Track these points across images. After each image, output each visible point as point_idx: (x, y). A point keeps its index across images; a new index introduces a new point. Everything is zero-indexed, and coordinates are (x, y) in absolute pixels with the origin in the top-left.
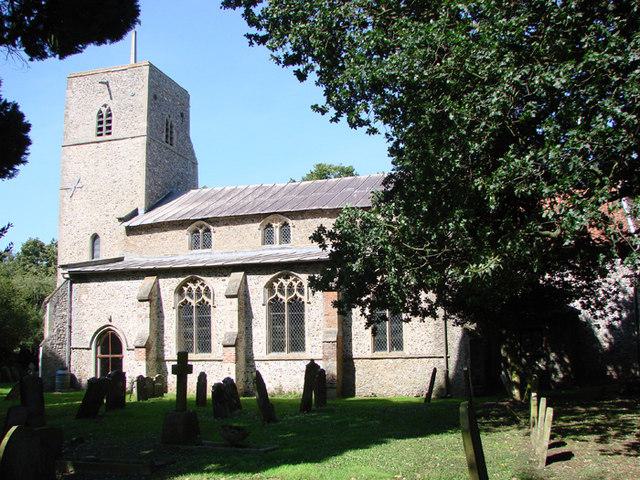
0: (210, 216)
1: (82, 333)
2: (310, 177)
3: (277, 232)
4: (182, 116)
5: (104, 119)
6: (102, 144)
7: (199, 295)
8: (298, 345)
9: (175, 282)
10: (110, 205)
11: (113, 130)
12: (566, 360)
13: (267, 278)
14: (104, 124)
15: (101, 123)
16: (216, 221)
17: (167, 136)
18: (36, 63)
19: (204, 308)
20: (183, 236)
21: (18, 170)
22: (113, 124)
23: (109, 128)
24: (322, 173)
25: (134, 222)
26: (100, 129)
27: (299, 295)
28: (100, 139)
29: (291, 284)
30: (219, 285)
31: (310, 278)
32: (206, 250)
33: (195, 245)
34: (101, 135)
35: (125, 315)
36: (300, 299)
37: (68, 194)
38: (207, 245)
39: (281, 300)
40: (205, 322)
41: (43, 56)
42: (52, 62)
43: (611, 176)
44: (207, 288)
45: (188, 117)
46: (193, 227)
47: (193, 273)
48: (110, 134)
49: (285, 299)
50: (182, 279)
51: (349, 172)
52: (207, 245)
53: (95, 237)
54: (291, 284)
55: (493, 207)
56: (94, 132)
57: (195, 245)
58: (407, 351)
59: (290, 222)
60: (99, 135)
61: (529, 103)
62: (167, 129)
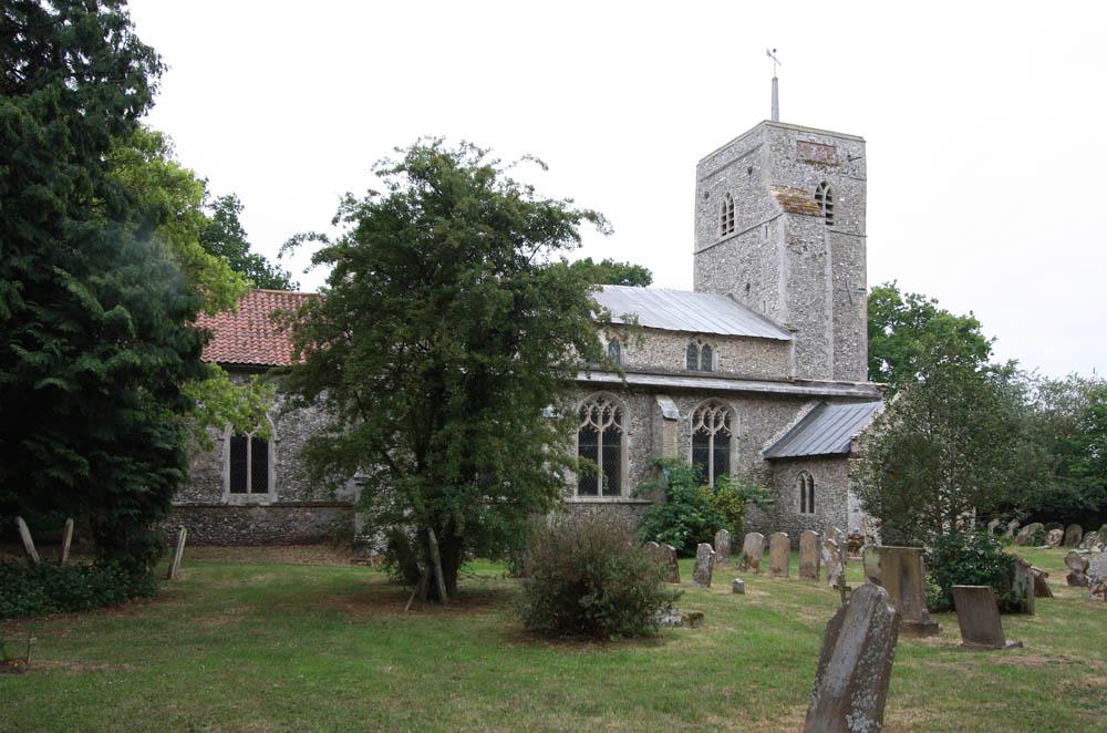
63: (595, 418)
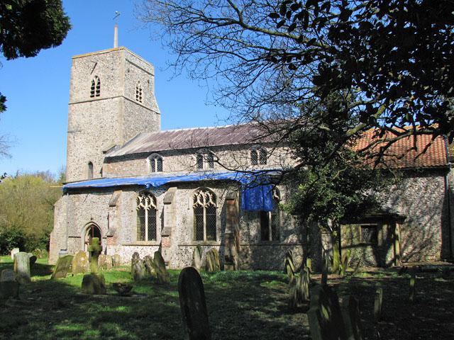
0: (161, 150)
5: (96, 89)
6: (93, 102)
10: (100, 143)
11: (101, 93)
12: (390, 33)
14: (96, 90)
15: (93, 88)
16: (166, 153)
18: (11, 61)
20: (192, 159)
22: (101, 89)
23: (98, 92)
25: (113, 154)
26: (93, 93)
28: (92, 99)
31: (325, 206)
37: (72, 136)
41: (16, 56)
42: (21, 61)
43: (367, 193)
46: (150, 156)
53: (91, 164)
55: (310, 150)
59: (164, 158)
60: (91, 97)
61: (389, 21)
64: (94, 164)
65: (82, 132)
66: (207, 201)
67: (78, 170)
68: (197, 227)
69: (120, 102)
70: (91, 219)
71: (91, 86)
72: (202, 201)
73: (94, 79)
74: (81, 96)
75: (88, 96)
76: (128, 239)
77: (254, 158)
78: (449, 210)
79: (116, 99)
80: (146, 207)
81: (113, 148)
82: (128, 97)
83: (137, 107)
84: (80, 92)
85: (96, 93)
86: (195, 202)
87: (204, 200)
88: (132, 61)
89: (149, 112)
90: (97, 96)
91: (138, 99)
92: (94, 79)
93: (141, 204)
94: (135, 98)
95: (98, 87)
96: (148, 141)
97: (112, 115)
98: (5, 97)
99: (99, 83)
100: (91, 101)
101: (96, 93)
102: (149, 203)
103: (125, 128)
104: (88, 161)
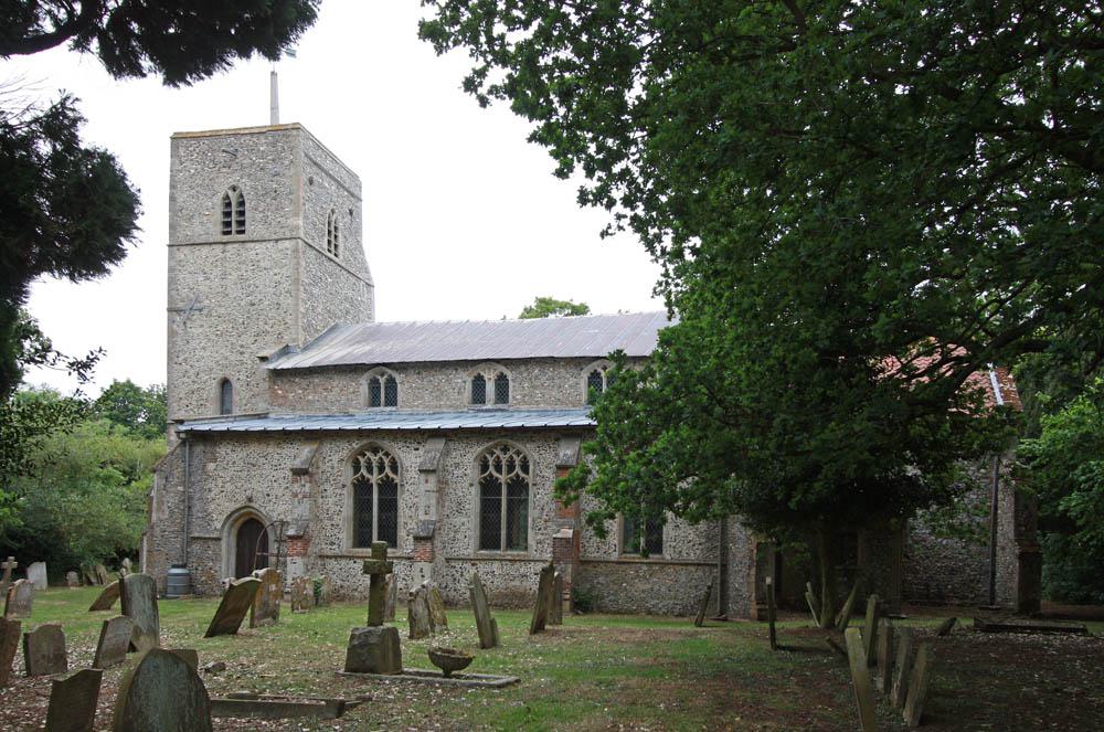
1: (208, 517)
2: (528, 313)
3: (490, 388)
4: (351, 213)
5: (234, 217)
6: (229, 247)
7: (511, 467)
8: (517, 539)
9: (344, 450)
10: (247, 339)
13: (478, 449)
15: (227, 214)
17: (329, 242)
19: (389, 489)
21: (108, 271)
22: (219, 217)
23: (242, 223)
24: (545, 307)
26: (228, 224)
27: (522, 475)
29: (511, 457)
30: (411, 459)
32: (389, 409)
33: (374, 401)
34: (229, 233)
35: (273, 493)
36: (368, 480)
38: (392, 400)
39: (497, 479)
40: (389, 506)
41: (137, 71)
44: (393, 459)
45: (360, 215)
47: (372, 439)
48: (243, 232)
49: (374, 479)
50: (487, 445)
51: (580, 310)
52: (392, 400)
54: (511, 457)
56: (220, 228)
57: (374, 401)
58: (667, 555)
60: (225, 233)
62: (329, 232)
63: (498, 468)
64: (236, 385)
65: (205, 312)
66: (509, 472)
67: (195, 397)
68: (625, 527)
69: (296, 251)
70: (250, 500)
71: (219, 210)
72: (370, 471)
73: (230, 193)
74: (199, 229)
75: (215, 230)
76: (332, 544)
77: (478, 395)
78: (996, 508)
79: (287, 244)
80: (374, 479)
81: (286, 351)
82: (310, 242)
83: (330, 267)
84: (196, 221)
85: (234, 227)
86: (355, 473)
87: (504, 468)
88: (318, 160)
89: (353, 280)
90: (240, 232)
91: (332, 248)
92: (230, 193)
93: (363, 471)
94: (326, 246)
95: (242, 213)
96: (358, 342)
97: (277, 278)
98: (466, 90)
99: (242, 204)
100: (225, 243)
101: (234, 227)
102: (381, 469)
103: (308, 309)
104: (220, 375)
